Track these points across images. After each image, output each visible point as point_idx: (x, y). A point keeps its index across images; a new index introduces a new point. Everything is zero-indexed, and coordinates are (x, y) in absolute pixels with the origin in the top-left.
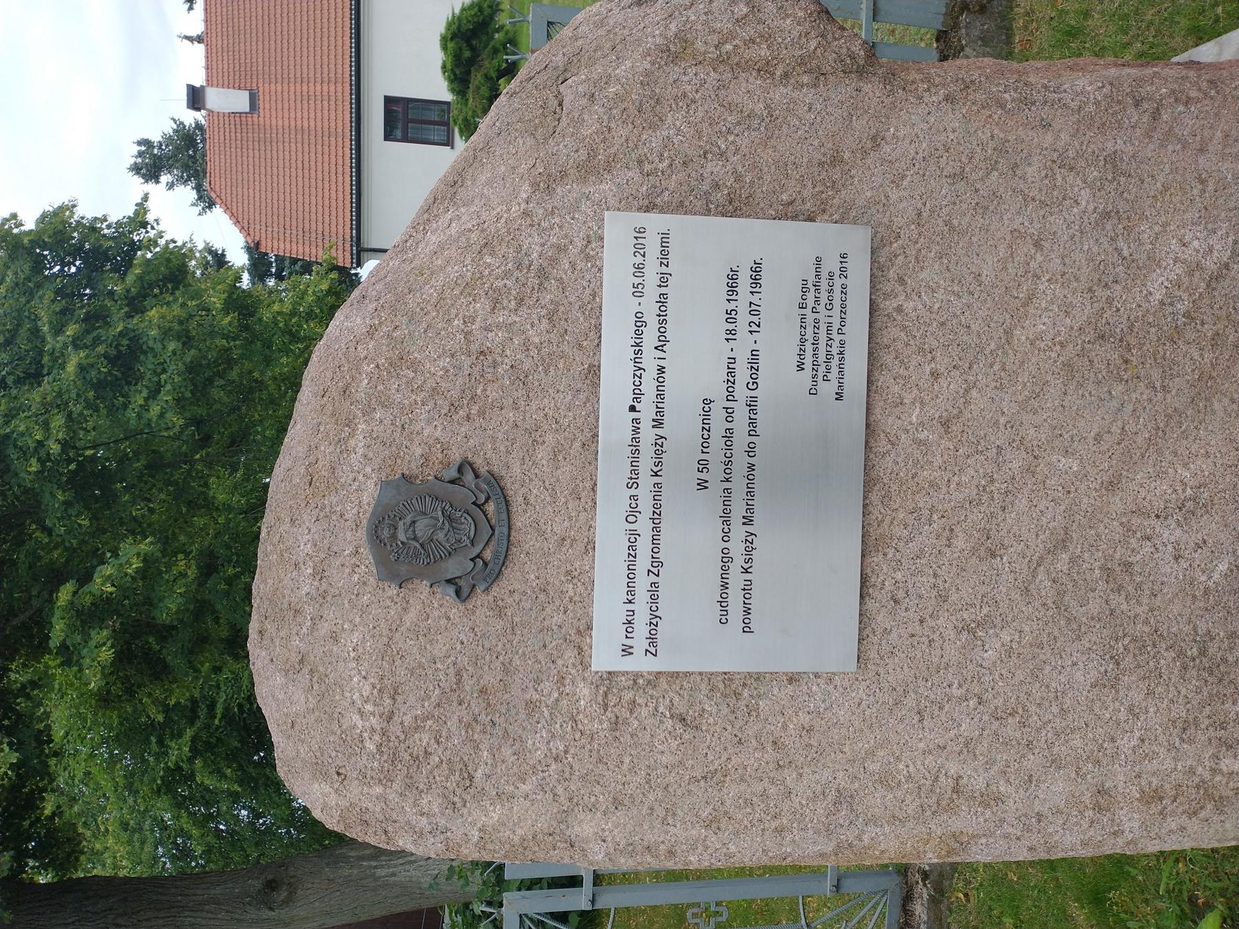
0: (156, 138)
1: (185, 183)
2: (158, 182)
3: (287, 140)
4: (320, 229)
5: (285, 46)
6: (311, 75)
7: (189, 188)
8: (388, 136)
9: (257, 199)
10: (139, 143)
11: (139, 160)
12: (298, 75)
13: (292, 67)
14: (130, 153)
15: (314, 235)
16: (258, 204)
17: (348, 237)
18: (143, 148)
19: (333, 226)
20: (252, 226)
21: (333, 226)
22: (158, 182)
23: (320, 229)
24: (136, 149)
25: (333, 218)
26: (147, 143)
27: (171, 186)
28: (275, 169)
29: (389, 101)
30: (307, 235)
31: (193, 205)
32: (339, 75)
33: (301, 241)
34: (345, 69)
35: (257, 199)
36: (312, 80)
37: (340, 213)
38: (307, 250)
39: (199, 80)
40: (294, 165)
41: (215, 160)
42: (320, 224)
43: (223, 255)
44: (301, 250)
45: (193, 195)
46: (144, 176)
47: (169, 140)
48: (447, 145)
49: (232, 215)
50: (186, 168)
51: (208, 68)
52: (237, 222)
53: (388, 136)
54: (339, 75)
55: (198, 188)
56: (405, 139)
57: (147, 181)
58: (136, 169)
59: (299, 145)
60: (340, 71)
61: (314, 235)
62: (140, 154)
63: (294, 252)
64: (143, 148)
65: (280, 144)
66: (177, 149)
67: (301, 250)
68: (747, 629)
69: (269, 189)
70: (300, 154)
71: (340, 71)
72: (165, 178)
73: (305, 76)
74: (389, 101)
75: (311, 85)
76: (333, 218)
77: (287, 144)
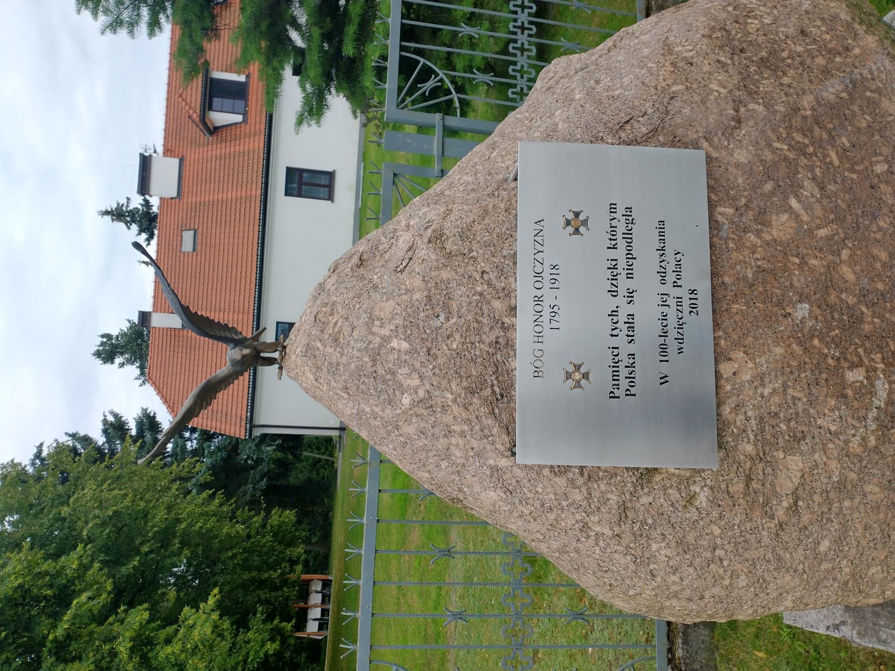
0: (115, 332)
1: (132, 364)
2: (113, 363)
3: (206, 348)
4: (224, 410)
5: (210, 287)
6: (227, 307)
7: (134, 366)
8: (288, 193)
9: (181, 386)
10: (103, 336)
11: (101, 348)
12: (218, 306)
13: (213, 301)
14: (95, 343)
15: (219, 415)
16: (181, 390)
17: (244, 417)
18: (105, 340)
19: (234, 409)
20: (176, 405)
21: (234, 409)
22: (113, 363)
23: (224, 410)
24: (99, 340)
25: (235, 403)
26: (108, 336)
27: (122, 365)
28: (196, 367)
29: (289, 170)
30: (215, 414)
31: (137, 378)
32: (246, 309)
33: (210, 418)
34: (252, 306)
35: (181, 386)
36: (227, 310)
37: (240, 400)
38: (214, 424)
39: (148, 308)
40: (209, 365)
41: (153, 355)
42: (225, 407)
43: (154, 417)
44: (209, 424)
45: (138, 371)
46: (103, 359)
47: (124, 335)
48: (329, 199)
49: (162, 397)
50: (133, 353)
51: (155, 297)
52: (165, 402)
53: (288, 193)
54: (246, 309)
55: (142, 368)
56: (299, 195)
57: (105, 363)
58: (98, 354)
59: (214, 353)
60: (247, 306)
61: (219, 415)
62: (102, 344)
63: (204, 425)
64: (105, 340)
65: (201, 351)
66: (129, 341)
67: (209, 424)
68: (613, 208)
69: (191, 380)
70: (214, 358)
71: (247, 306)
72: (118, 360)
73: (222, 307)
74: (289, 170)
75: (226, 314)
76: (235, 403)
77: (206, 351)
